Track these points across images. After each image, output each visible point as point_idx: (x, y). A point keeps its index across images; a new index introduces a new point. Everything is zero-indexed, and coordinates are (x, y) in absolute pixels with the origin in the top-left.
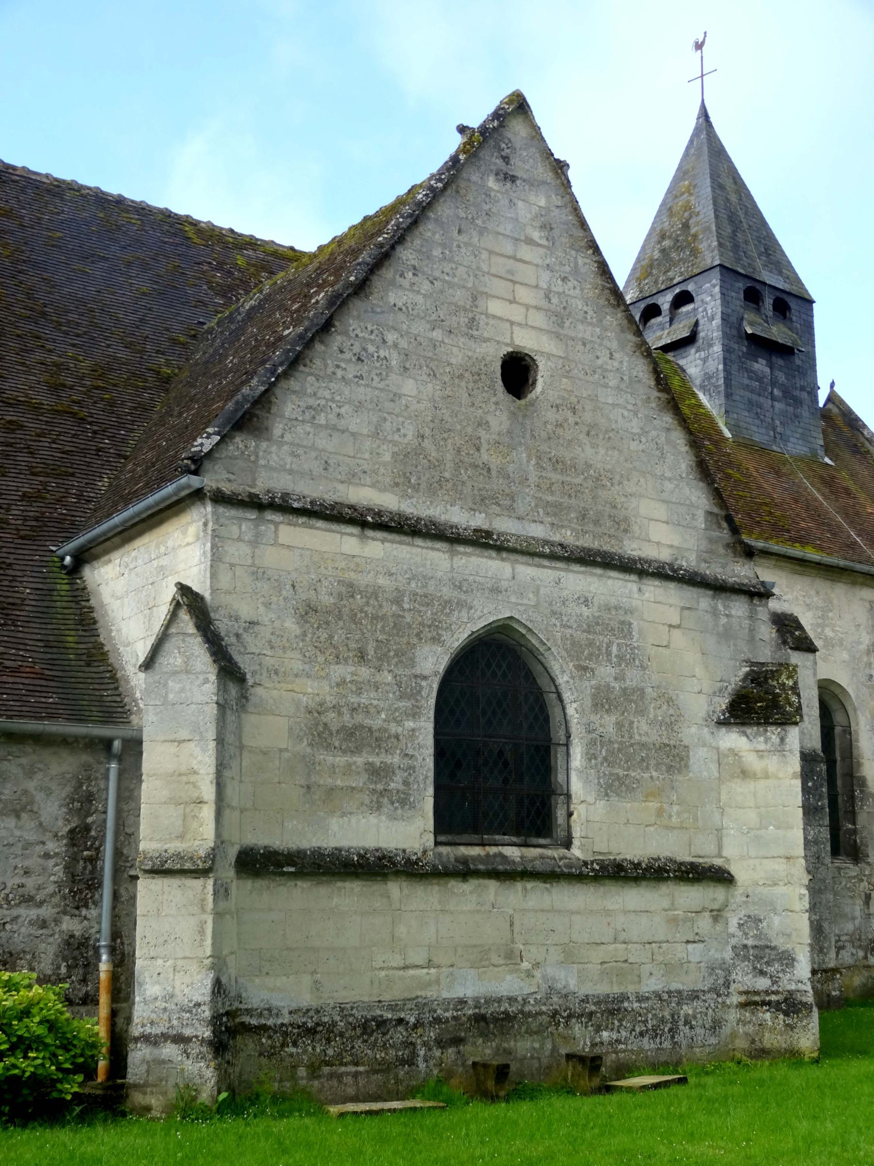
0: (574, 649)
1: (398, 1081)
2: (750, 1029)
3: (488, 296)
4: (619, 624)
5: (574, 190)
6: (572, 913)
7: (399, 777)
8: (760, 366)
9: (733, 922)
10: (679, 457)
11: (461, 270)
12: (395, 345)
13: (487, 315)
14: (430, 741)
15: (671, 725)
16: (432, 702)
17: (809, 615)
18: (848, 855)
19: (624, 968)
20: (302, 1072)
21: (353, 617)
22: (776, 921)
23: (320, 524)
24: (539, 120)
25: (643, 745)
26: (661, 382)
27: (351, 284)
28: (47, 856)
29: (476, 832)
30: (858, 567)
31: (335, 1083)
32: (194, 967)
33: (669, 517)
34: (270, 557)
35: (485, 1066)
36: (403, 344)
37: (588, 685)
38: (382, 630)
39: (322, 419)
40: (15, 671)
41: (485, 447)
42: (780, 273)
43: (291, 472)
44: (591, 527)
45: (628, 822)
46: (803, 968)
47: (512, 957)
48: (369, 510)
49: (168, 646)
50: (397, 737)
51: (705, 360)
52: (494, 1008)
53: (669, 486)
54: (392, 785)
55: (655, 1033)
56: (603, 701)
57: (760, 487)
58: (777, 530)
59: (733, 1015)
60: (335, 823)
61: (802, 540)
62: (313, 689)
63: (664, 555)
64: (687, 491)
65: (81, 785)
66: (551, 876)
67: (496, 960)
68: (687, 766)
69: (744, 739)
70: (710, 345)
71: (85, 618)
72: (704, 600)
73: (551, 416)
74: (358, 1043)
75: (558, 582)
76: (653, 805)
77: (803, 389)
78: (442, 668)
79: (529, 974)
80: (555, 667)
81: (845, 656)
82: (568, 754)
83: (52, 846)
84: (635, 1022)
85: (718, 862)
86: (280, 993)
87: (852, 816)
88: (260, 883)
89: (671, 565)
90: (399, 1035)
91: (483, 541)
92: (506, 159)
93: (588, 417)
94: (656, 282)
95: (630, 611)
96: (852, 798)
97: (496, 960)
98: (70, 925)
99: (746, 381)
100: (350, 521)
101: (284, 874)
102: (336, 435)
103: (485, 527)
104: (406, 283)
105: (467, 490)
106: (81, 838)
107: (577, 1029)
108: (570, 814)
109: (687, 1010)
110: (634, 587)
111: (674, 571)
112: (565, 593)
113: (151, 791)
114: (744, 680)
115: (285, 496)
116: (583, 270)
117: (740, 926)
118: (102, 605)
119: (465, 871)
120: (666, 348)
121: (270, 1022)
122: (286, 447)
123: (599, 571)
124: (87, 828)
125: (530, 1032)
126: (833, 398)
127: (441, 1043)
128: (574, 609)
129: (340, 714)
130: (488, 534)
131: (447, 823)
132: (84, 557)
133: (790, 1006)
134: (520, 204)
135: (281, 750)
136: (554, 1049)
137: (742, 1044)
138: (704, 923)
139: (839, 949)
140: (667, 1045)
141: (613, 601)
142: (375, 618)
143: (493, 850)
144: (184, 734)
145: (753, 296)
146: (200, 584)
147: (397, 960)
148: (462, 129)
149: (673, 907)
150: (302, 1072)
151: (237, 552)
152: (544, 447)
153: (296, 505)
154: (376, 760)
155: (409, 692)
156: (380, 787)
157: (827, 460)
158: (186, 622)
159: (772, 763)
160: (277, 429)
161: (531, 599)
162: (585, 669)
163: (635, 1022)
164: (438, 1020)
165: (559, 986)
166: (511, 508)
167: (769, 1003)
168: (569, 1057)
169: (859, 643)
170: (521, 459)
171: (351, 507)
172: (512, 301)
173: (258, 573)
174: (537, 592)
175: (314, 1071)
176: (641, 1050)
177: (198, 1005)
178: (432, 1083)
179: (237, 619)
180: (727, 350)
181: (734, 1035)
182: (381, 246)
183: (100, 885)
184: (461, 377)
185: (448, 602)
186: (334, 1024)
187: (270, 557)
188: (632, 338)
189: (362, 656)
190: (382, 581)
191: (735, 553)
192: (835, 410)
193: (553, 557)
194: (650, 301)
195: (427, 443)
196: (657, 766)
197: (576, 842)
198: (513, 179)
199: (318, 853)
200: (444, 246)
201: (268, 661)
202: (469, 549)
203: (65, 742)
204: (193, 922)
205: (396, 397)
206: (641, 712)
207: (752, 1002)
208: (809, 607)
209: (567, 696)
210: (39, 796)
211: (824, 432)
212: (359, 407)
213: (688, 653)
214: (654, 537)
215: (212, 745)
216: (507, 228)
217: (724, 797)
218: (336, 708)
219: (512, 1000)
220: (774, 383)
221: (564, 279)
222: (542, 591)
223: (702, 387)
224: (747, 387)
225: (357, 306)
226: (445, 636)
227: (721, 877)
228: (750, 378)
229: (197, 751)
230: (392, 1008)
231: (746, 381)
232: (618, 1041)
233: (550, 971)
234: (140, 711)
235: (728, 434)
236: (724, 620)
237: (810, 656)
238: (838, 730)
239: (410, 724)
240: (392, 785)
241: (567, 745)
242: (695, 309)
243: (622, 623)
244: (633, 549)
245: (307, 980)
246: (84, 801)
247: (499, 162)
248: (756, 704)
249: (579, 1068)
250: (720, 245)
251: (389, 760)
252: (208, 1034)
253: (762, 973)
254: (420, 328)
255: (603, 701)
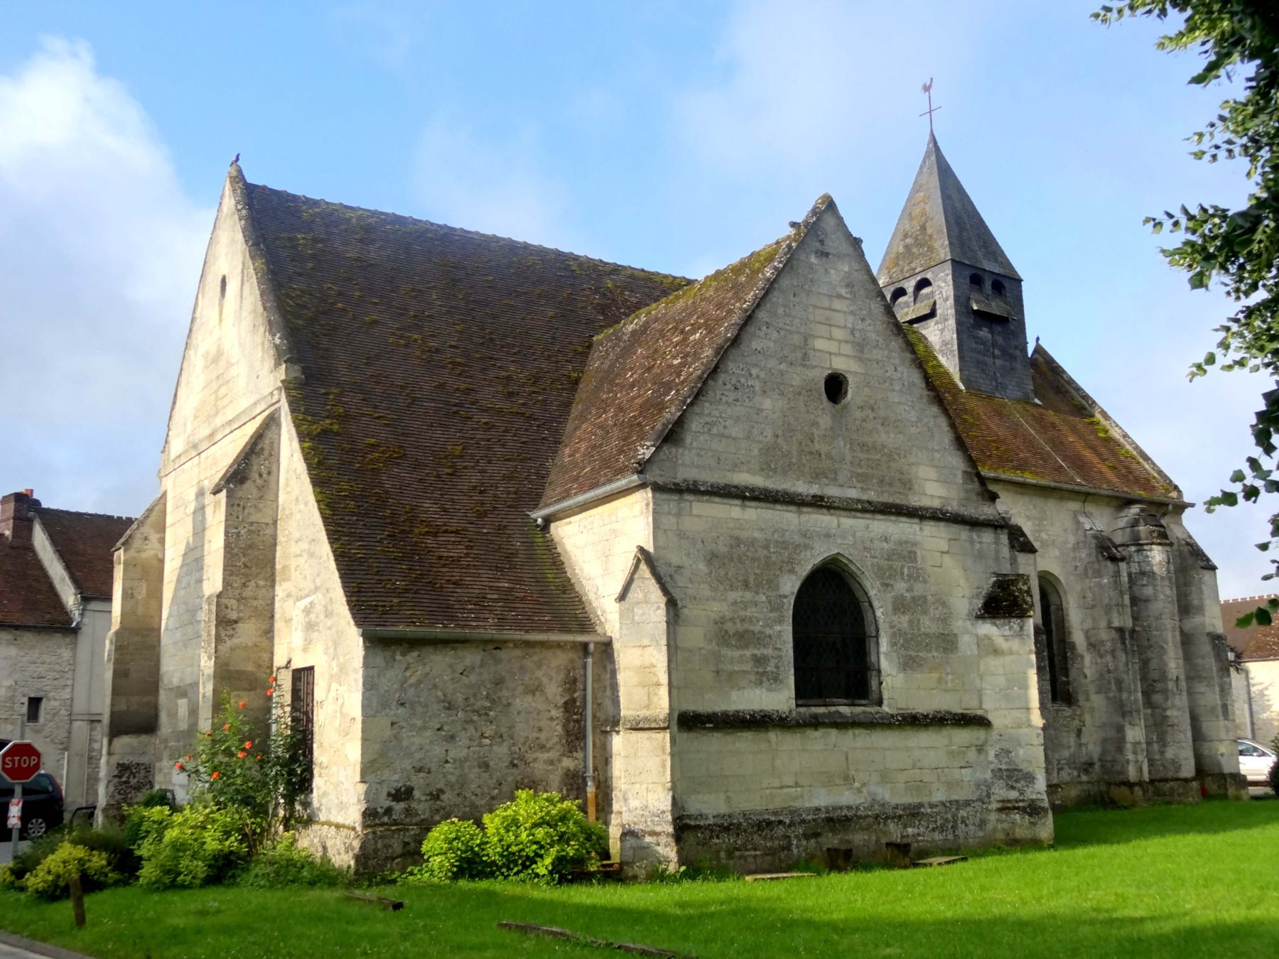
0: (880, 572)
1: (781, 861)
2: (1005, 825)
3: (815, 337)
4: (907, 553)
5: (867, 257)
6: (885, 749)
7: (773, 663)
8: (984, 333)
9: (992, 753)
10: (943, 435)
11: (797, 321)
12: (758, 377)
13: (814, 350)
14: (790, 639)
15: (945, 620)
16: (791, 612)
17: (1030, 523)
18: (1063, 700)
19: (919, 786)
20: (723, 855)
21: (740, 559)
22: (1021, 752)
23: (717, 499)
24: (842, 212)
25: (927, 635)
26: (910, 347)
27: (729, 339)
28: (551, 719)
29: (820, 697)
30: (1065, 486)
31: (742, 861)
32: (660, 789)
33: (936, 479)
34: (689, 524)
35: (836, 850)
36: (762, 375)
37: (889, 597)
38: (758, 567)
39: (715, 431)
40: (523, 599)
41: (817, 439)
42: (996, 260)
43: (697, 467)
44: (887, 488)
45: (919, 688)
46: (1041, 784)
47: (848, 779)
48: (747, 488)
49: (634, 586)
50: (770, 637)
51: (942, 331)
52: (838, 813)
53: (937, 455)
54: (769, 669)
55: (942, 829)
56: (900, 606)
57: (988, 427)
58: (1002, 461)
59: (993, 817)
60: (734, 695)
61: (1022, 467)
62: (718, 608)
63: (936, 504)
64: (950, 458)
65: (569, 672)
66: (871, 724)
67: (838, 781)
68: (956, 648)
69: (995, 628)
70: (946, 320)
71: (554, 561)
72: (964, 533)
73: (858, 414)
74: (756, 837)
75: (867, 527)
76: (935, 675)
77: (1016, 347)
78: (796, 590)
79: (859, 790)
80: (867, 584)
81: (1057, 553)
82: (878, 643)
83: (554, 713)
84: (929, 822)
85: (980, 712)
86: (710, 805)
87: (1066, 671)
88: (692, 735)
89: (941, 510)
90: (780, 831)
91: (818, 503)
92: (822, 242)
93: (882, 413)
94: (902, 271)
95: (915, 544)
96: (1065, 658)
97: (838, 781)
98: (568, 763)
99: (974, 346)
100: (737, 497)
101: (705, 728)
102: (724, 440)
103: (819, 493)
104: (762, 334)
105: (807, 469)
106: (572, 708)
107: (892, 826)
108: (881, 683)
109: (963, 813)
110: (917, 527)
111: (944, 514)
112: (872, 535)
113: (626, 679)
114: (993, 586)
115: (695, 482)
116: (875, 312)
117: (996, 756)
118: (566, 551)
119: (815, 723)
120: (912, 322)
121: (702, 823)
122: (694, 451)
123: (893, 518)
124: (574, 701)
125: (862, 829)
126: (1039, 350)
127: (806, 836)
128: (879, 545)
129: (735, 623)
130: (822, 498)
131: (803, 693)
132: (548, 521)
133: (1033, 810)
134: (832, 271)
135: (700, 649)
136: (878, 841)
137: (1000, 836)
138: (972, 755)
139: (1060, 770)
140: (950, 837)
141: (904, 538)
142: (753, 559)
143: (833, 709)
144: (646, 642)
145: (976, 280)
146: (650, 548)
147: (776, 783)
148: (793, 225)
149: (951, 743)
150: (723, 855)
151: (670, 522)
152: (854, 436)
153: (702, 489)
154: (758, 652)
155: (776, 607)
156: (761, 670)
157: (1037, 401)
158: (644, 569)
159: (1015, 644)
160: (688, 440)
161: (850, 540)
162: (887, 585)
163: (929, 822)
164: (803, 821)
165: (878, 798)
166: (835, 479)
167: (1018, 808)
168: (888, 844)
169: (1066, 542)
170: (841, 446)
171: (736, 487)
172: (830, 339)
173: (681, 535)
174: (854, 535)
175: (730, 854)
176: (933, 841)
177: (663, 812)
178: (802, 860)
179: (670, 565)
180: (959, 323)
181: (995, 830)
182: (746, 311)
183: (585, 737)
184: (799, 394)
185: (799, 546)
186: (740, 824)
187: (689, 524)
188: (909, 355)
189: (746, 585)
190: (757, 535)
191: (984, 499)
192: (1041, 359)
193: (864, 511)
194: (898, 285)
195: (780, 440)
196: (937, 649)
197: (885, 702)
198: (827, 255)
199: (725, 715)
200: (785, 306)
201: (690, 592)
202: (810, 510)
203: (559, 645)
204: (658, 760)
205: (759, 411)
206: (925, 612)
207: (1006, 808)
208: (1028, 518)
209: (876, 604)
210: (545, 680)
211: (1033, 379)
212: (737, 420)
213: (953, 570)
214: (929, 492)
215: (665, 648)
216: (824, 289)
217: (982, 668)
218: (732, 619)
219: (849, 808)
220: (994, 345)
221: (863, 320)
222: (858, 534)
223: (941, 351)
224: (974, 350)
225: (734, 353)
226: (797, 568)
227: (981, 722)
228: (977, 343)
229: (655, 652)
230: (775, 813)
231: (974, 346)
232: (918, 834)
233: (872, 788)
234: (602, 623)
235: (962, 387)
236: (977, 546)
237: (1031, 556)
238: (1053, 608)
239: (778, 628)
240: (769, 669)
241: (877, 637)
242: (932, 292)
243: (910, 552)
244: (915, 501)
245: (722, 797)
246: (572, 683)
247: (817, 244)
248: (1001, 602)
249: (896, 852)
250: (951, 244)
251: (765, 652)
252: (670, 829)
253: (1013, 788)
254: (772, 363)
255: (900, 606)
